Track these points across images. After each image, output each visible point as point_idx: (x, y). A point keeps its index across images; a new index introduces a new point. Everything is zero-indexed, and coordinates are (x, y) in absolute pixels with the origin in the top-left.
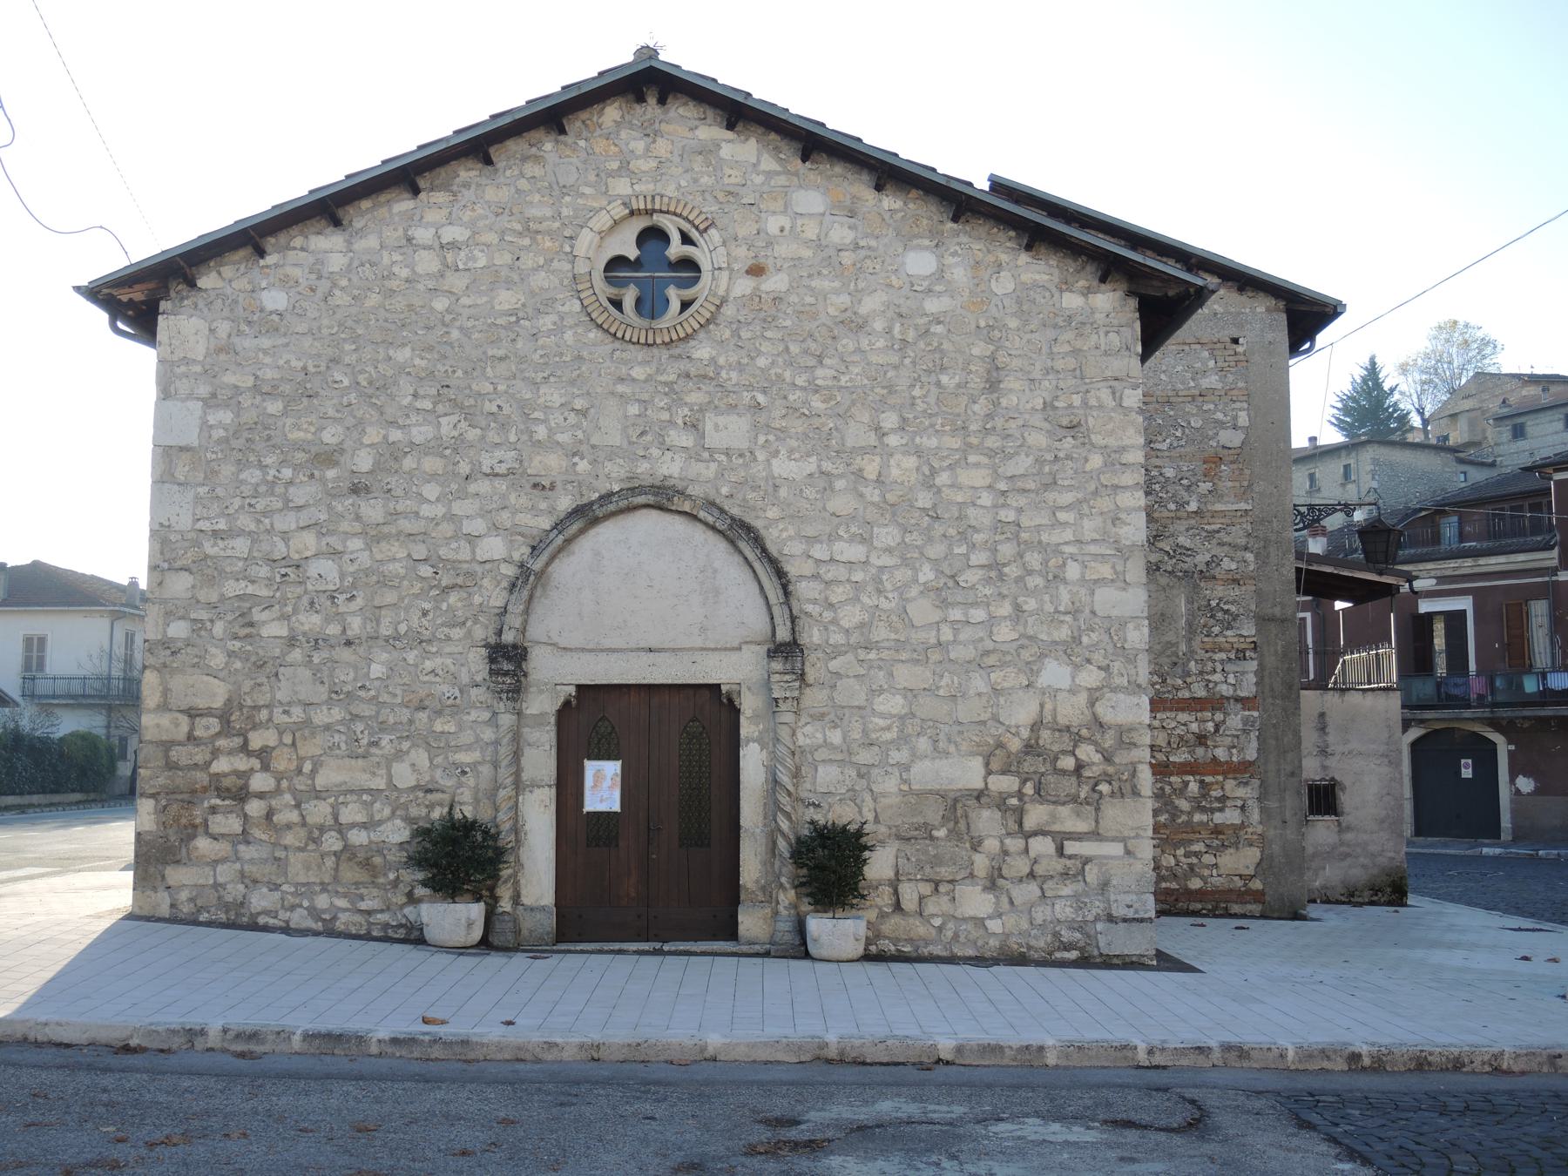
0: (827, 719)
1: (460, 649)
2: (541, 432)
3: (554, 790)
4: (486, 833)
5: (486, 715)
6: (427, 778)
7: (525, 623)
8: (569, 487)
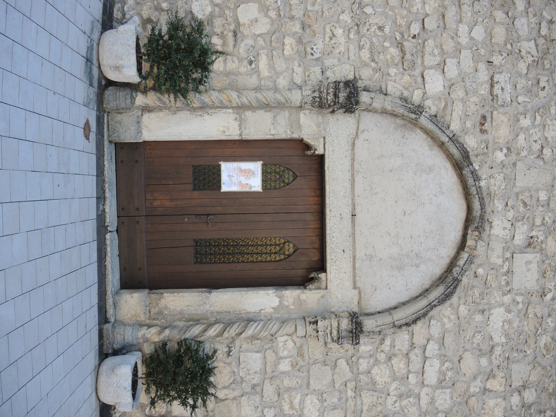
0: (299, 359)
1: (352, 58)
2: (525, 122)
3: (237, 138)
4: (200, 82)
5: (298, 80)
6: (246, 33)
7: (375, 111)
8: (483, 145)
